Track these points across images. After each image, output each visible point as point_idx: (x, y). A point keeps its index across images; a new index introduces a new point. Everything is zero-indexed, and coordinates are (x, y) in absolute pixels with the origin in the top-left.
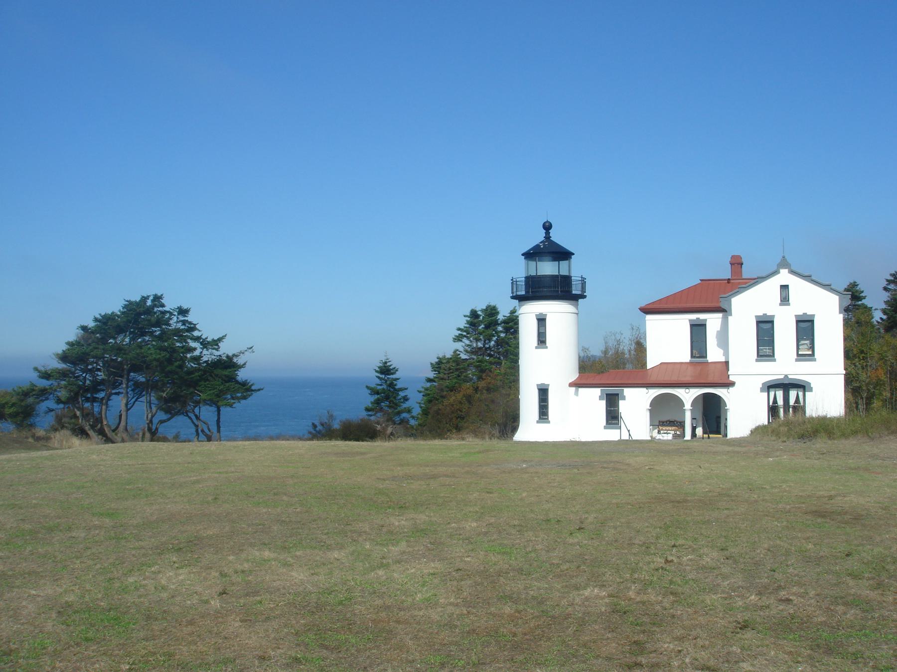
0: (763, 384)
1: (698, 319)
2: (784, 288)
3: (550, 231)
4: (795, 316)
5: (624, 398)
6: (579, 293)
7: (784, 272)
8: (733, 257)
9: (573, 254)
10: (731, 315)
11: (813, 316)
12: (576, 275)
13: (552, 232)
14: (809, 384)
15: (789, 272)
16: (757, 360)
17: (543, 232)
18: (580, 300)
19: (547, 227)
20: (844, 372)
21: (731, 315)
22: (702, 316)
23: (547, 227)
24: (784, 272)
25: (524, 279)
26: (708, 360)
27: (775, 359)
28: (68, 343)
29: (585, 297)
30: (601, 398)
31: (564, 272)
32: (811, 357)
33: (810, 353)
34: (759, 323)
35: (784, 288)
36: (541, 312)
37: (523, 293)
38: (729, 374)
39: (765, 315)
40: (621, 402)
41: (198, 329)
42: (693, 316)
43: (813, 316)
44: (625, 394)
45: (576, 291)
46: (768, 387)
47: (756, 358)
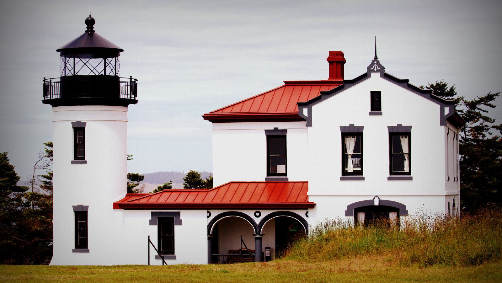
0: (349, 207)
1: (276, 129)
2: (376, 98)
3: (93, 26)
4: (388, 126)
5: (180, 223)
6: (128, 97)
7: (376, 77)
8: (331, 53)
9: (122, 51)
10: (354, 125)
11: (362, 128)
12: (124, 75)
13: (96, 27)
14: (404, 207)
15: (381, 76)
16: (341, 179)
17: (84, 28)
18: (130, 106)
19: (90, 22)
21: (354, 125)
22: (281, 126)
23: (90, 22)
24: (376, 77)
25: (59, 80)
26: (288, 179)
27: (412, 177)
28: (398, 124)
29: (135, 102)
30: (152, 223)
31: (109, 72)
32: (358, 175)
33: (359, 169)
35: (376, 98)
36: (78, 120)
37: (58, 97)
38: (308, 194)
39: (352, 126)
40: (177, 228)
41: (494, 95)
42: (271, 126)
43: (362, 128)
44: (182, 217)
45: (124, 94)
46: (355, 209)
47: (388, 175)
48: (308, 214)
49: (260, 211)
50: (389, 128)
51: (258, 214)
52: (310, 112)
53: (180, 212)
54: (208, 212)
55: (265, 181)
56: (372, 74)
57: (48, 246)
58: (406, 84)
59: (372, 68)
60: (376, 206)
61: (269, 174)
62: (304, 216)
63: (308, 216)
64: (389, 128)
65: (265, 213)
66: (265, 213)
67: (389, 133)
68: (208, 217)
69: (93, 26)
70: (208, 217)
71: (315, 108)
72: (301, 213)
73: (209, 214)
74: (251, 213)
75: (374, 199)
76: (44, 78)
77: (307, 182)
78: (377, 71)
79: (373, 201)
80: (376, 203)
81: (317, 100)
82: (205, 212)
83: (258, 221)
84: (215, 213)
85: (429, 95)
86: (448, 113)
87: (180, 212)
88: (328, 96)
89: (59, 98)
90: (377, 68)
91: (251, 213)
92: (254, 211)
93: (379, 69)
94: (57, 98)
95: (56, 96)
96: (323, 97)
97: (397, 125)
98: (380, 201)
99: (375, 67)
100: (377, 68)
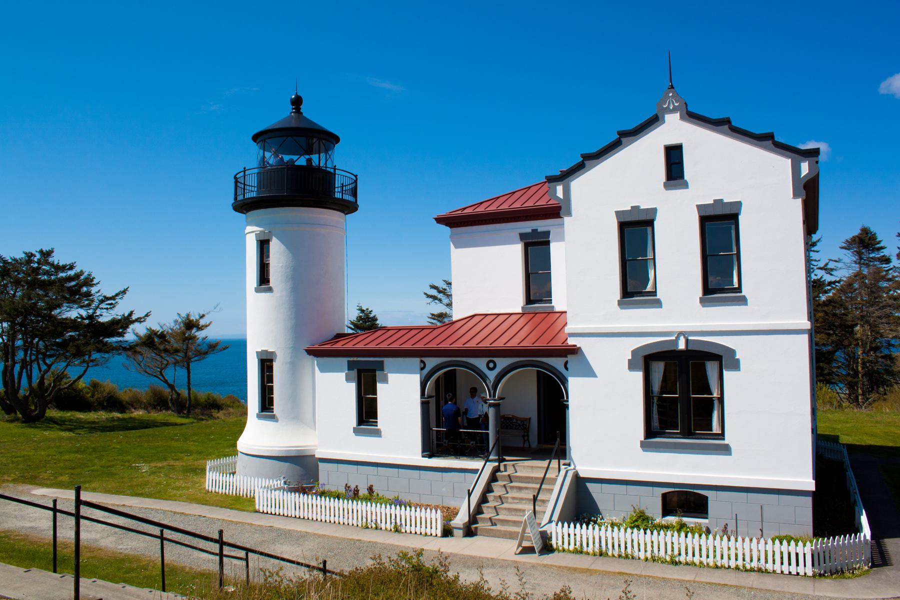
1: (535, 231)
11: (738, 204)
14: (732, 352)
19: (297, 102)
20: (806, 324)
23: (297, 102)
28: (632, 207)
34: (705, 220)
39: (635, 209)
42: (527, 226)
48: (568, 366)
49: (495, 359)
50: (618, 213)
51: (491, 365)
52: (567, 192)
53: (383, 361)
54: (422, 361)
55: (521, 312)
56: (668, 117)
57: (51, 316)
58: (726, 127)
59: (665, 104)
60: (681, 351)
61: (529, 300)
62: (561, 368)
63: (567, 369)
64: (618, 213)
65: (502, 363)
66: (502, 363)
67: (700, 216)
68: (422, 369)
69: (301, 107)
70: (422, 369)
71: (579, 185)
72: (557, 363)
73: (422, 365)
74: (480, 363)
75: (678, 338)
76: (245, 168)
77: (566, 312)
78: (674, 110)
79: (676, 342)
80: (682, 346)
81: (578, 169)
82: (417, 360)
83: (492, 375)
84: (432, 362)
85: (771, 142)
86: (807, 172)
87: (383, 361)
88: (597, 160)
89: (255, 196)
90: (673, 104)
91: (480, 363)
92: (485, 360)
93: (676, 105)
94: (252, 196)
95: (252, 194)
96: (587, 163)
97: (630, 209)
98: (687, 341)
99: (669, 102)
100: (673, 104)
